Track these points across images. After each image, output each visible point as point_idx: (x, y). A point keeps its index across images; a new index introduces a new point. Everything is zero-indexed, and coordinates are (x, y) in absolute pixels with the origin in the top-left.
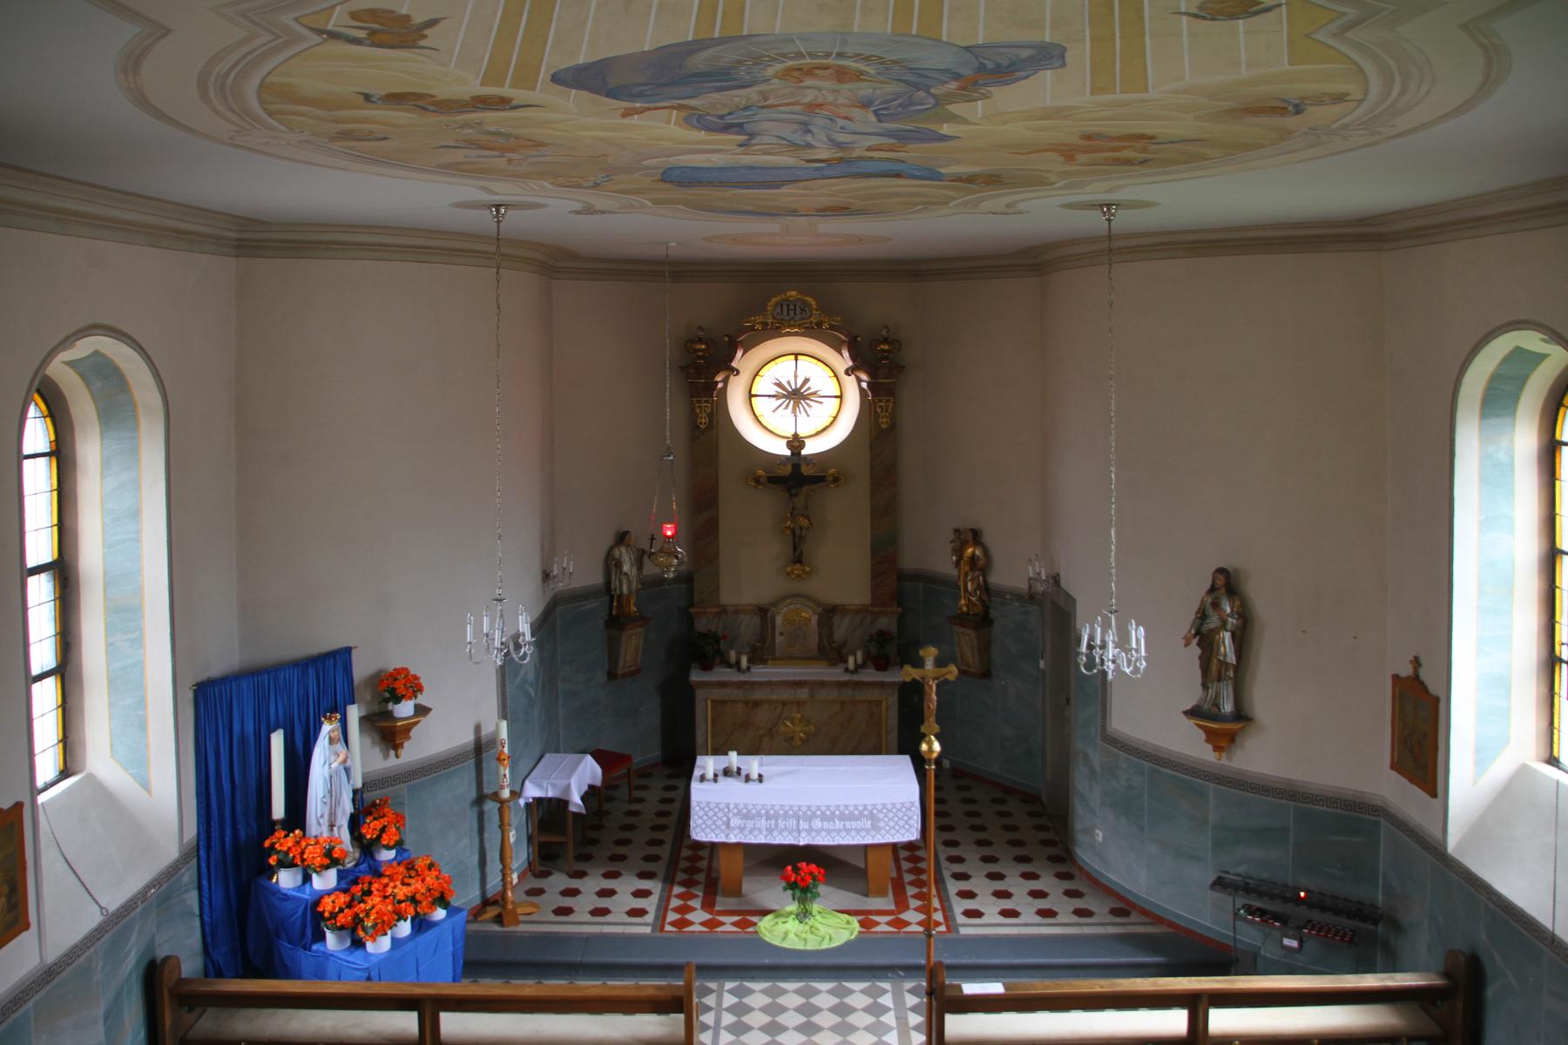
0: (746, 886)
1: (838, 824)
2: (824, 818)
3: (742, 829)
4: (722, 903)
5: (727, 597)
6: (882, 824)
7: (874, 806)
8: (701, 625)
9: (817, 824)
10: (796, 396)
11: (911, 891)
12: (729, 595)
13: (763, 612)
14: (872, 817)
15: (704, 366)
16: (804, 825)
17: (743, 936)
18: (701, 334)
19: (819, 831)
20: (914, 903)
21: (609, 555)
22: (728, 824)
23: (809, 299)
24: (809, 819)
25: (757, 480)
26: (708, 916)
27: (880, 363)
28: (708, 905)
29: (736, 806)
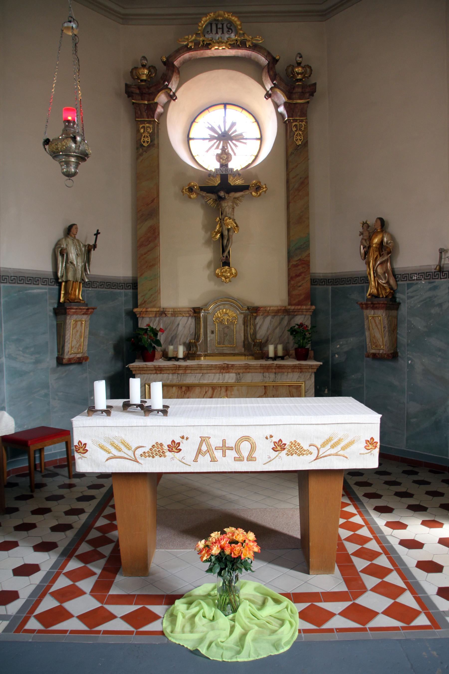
4: (121, 585)
5: (167, 301)
8: (143, 324)
10: (225, 137)
12: (167, 301)
13: (196, 312)
15: (144, 95)
18: (145, 62)
20: (371, 581)
21: (58, 244)
23: (234, 19)
25: (191, 190)
27: (296, 90)
28: (101, 589)
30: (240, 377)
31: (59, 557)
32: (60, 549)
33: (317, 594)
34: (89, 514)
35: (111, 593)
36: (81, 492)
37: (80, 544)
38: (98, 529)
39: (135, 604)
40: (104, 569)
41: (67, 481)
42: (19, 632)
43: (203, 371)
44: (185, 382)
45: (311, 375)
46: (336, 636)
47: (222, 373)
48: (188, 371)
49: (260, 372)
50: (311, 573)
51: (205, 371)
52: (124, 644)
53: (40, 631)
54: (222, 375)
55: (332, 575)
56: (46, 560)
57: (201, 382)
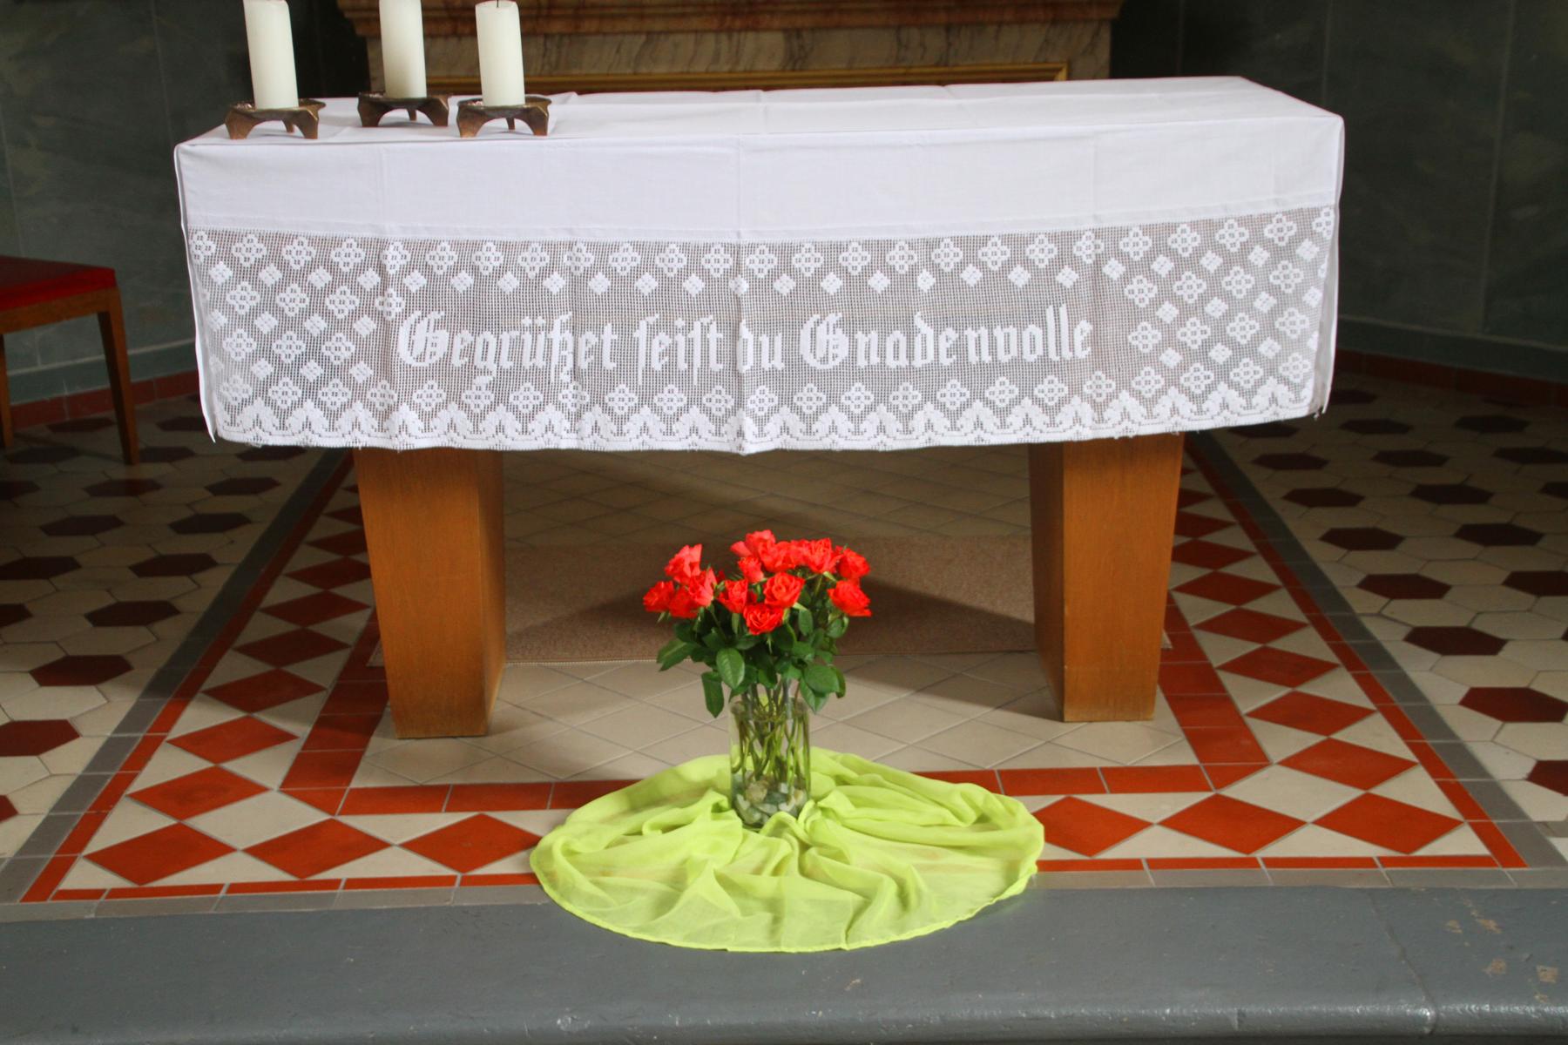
0: (510, 694)
1: (933, 343)
2: (859, 311)
3: (454, 379)
4: (386, 759)
6: (1145, 337)
7: (1111, 237)
9: (826, 342)
11: (1250, 695)
14: (1098, 297)
16: (759, 350)
17: (459, 897)
19: (833, 382)
20: (1282, 741)
22: (385, 366)
24: (787, 318)
26: (305, 816)
28: (318, 773)
29: (419, 252)
30: (802, 47)
31: (142, 696)
32: (145, 672)
33: (1090, 773)
34: (232, 569)
35: (358, 782)
36: (188, 505)
37: (220, 655)
38: (279, 611)
39: (448, 810)
40: (321, 724)
41: (119, 473)
42: (45, 899)
43: (649, 25)
44: (576, 71)
45: (1096, 34)
46: (1150, 878)
47: (730, 31)
48: (589, 25)
49: (886, 27)
50: (1067, 718)
51: (658, 25)
52: (426, 909)
53: (116, 893)
54: (730, 38)
55: (1149, 724)
56: (98, 713)
57: (644, 70)
